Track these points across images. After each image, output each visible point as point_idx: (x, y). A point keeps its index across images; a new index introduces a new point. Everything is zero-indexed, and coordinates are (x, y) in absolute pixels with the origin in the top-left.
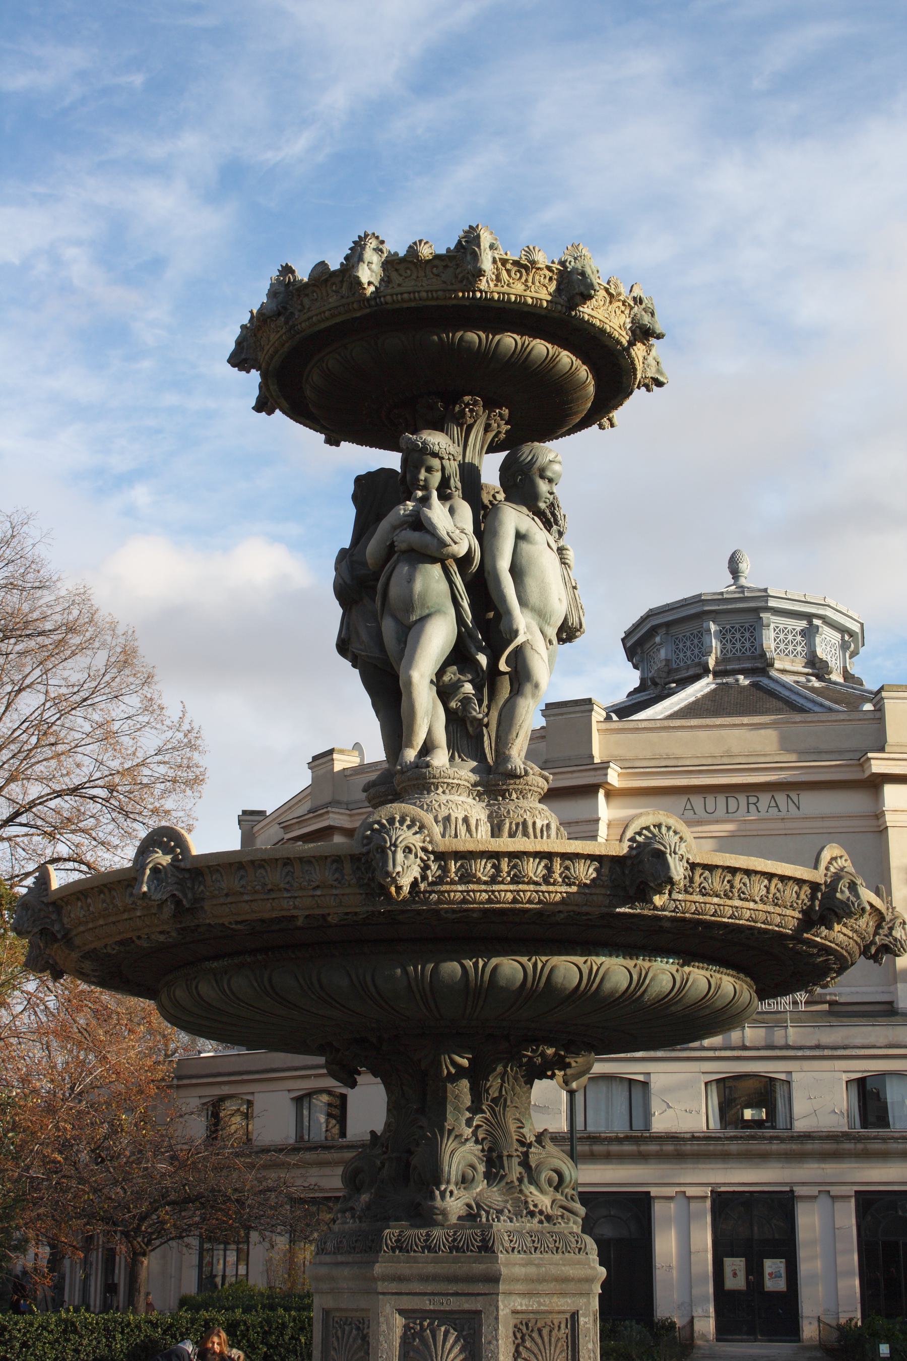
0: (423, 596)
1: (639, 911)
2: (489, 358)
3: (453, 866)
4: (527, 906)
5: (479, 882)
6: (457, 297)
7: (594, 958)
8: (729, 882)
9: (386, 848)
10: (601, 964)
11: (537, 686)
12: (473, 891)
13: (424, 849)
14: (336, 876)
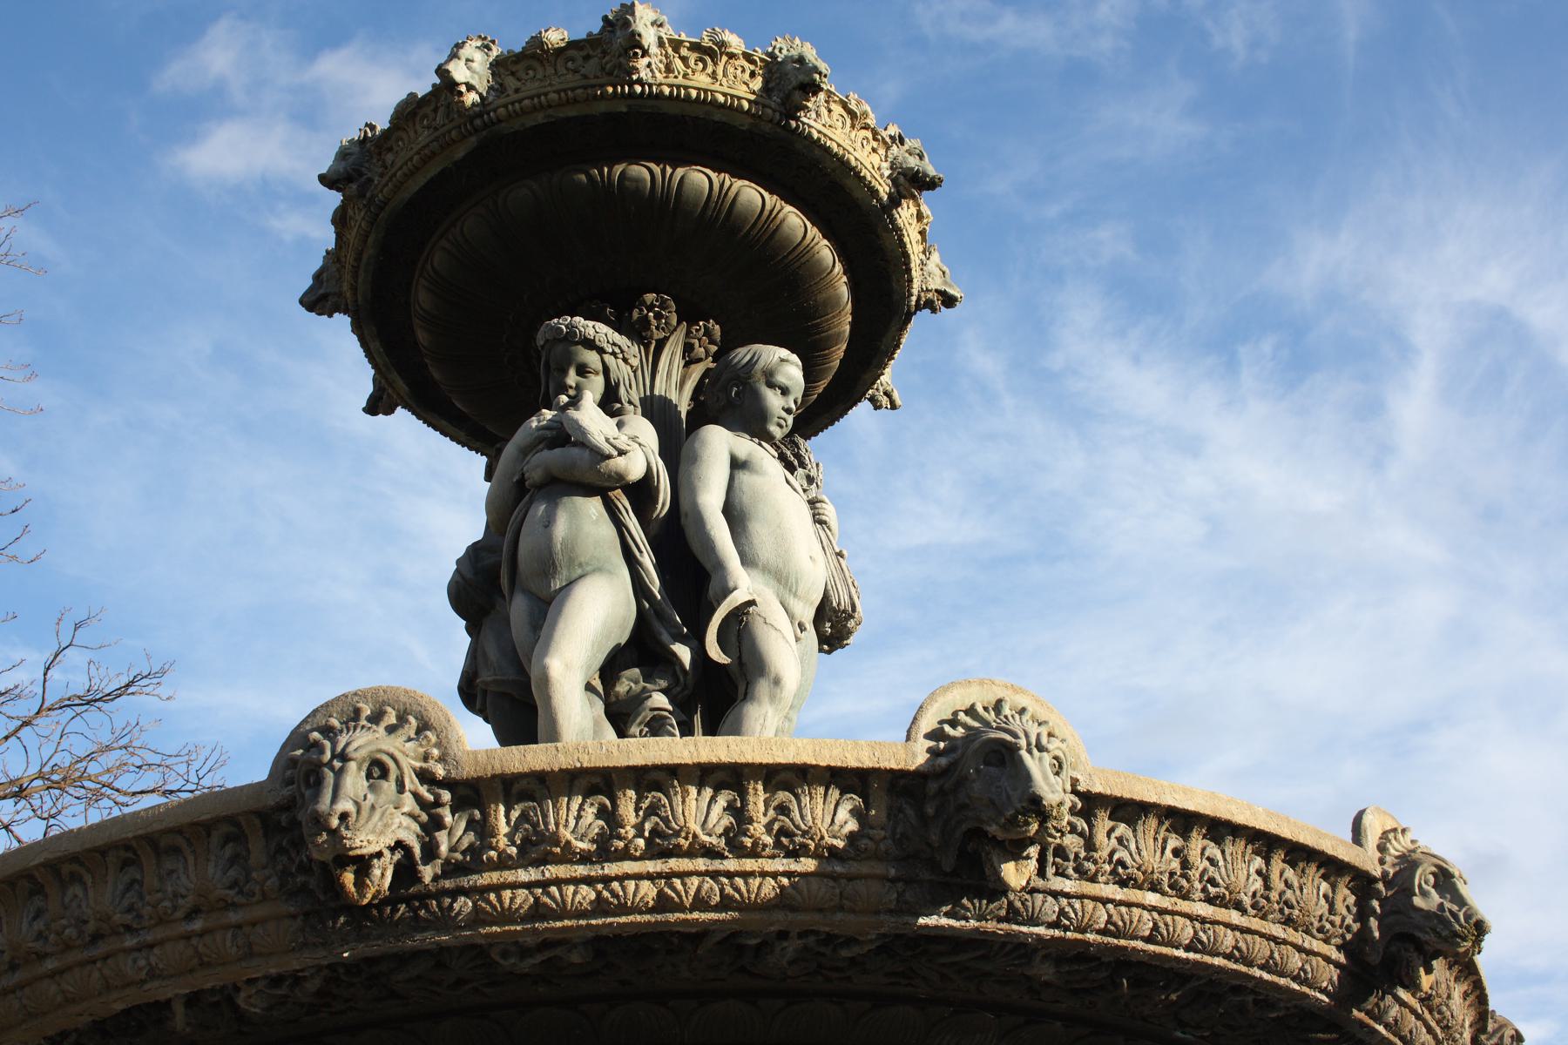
0: (570, 546)
1: (973, 923)
2: (668, 207)
4: (696, 915)
6: (604, 93)
8: (1176, 852)
9: (321, 765)
11: (777, 682)
12: (558, 882)
13: (425, 776)
14: (232, 873)
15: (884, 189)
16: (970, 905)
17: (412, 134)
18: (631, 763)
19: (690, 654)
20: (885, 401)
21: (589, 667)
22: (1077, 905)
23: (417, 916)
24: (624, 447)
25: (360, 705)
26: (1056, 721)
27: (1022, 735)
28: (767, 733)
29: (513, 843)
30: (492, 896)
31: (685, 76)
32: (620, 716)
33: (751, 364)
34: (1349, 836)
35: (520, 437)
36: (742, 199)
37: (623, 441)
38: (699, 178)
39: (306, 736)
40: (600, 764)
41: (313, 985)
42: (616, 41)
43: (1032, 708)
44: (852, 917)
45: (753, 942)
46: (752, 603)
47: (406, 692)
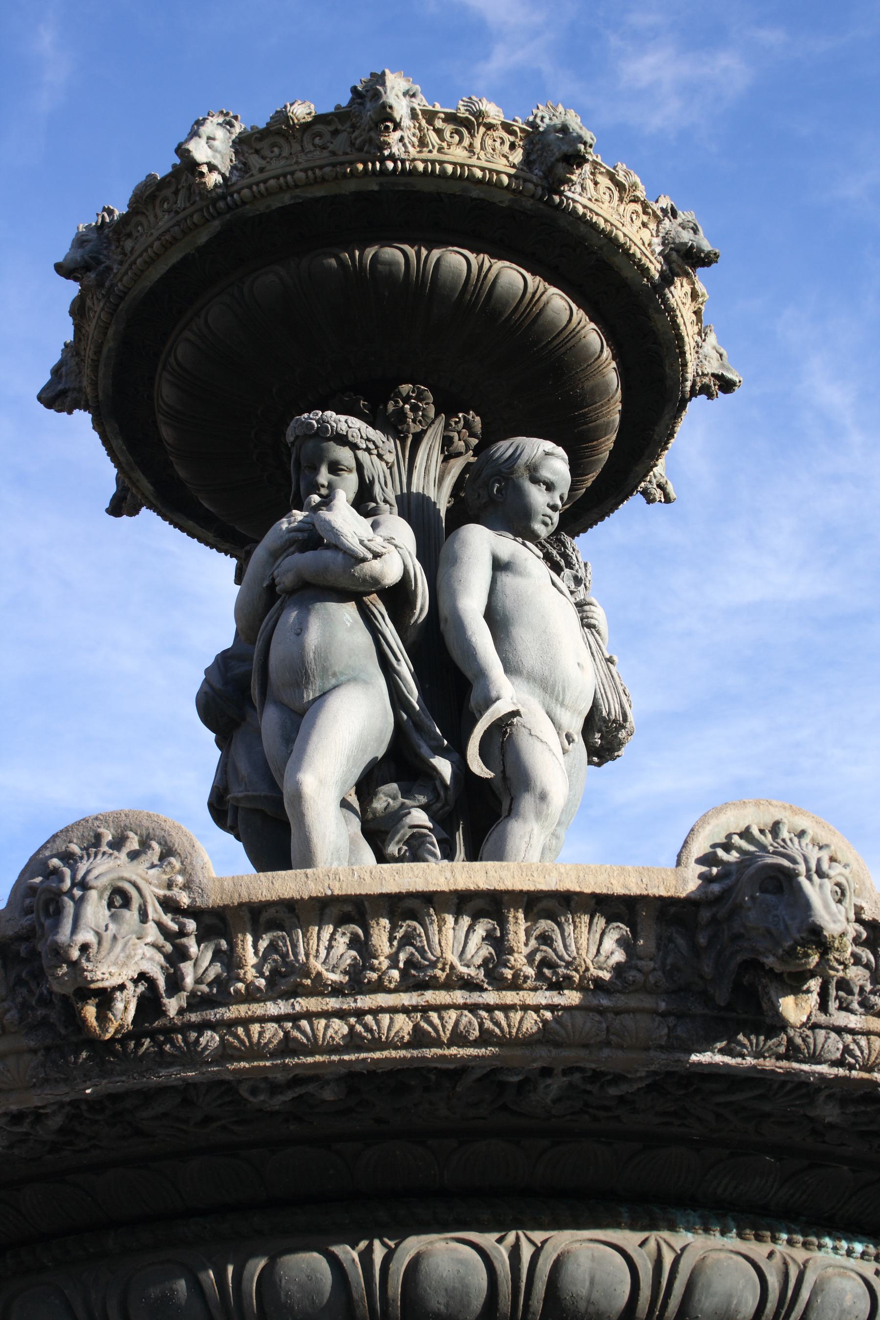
0: (323, 656)
1: (750, 1061)
3: (249, 951)
4: (454, 1051)
5: (319, 988)
6: (354, 172)
7: (666, 1234)
9: (61, 893)
10: (683, 1249)
11: (543, 797)
12: (309, 1016)
13: (169, 905)
15: (655, 267)
16: (746, 1042)
17: (152, 219)
18: (384, 891)
19: (451, 772)
20: (658, 494)
21: (344, 782)
22: (863, 1042)
23: (162, 1052)
24: (379, 549)
25: (101, 830)
26: (839, 844)
27: (800, 860)
28: (537, 853)
29: (262, 975)
30: (240, 1030)
31: (440, 150)
32: (377, 833)
33: (514, 458)
34: (766, 1255)
35: (269, 541)
36: (503, 281)
37: (378, 543)
38: (456, 260)
39: (45, 863)
40: (351, 891)
41: (56, 1122)
42: (366, 112)
43: (812, 830)
44: (620, 1053)
45: (515, 1079)
46: (516, 713)
47: (149, 816)
